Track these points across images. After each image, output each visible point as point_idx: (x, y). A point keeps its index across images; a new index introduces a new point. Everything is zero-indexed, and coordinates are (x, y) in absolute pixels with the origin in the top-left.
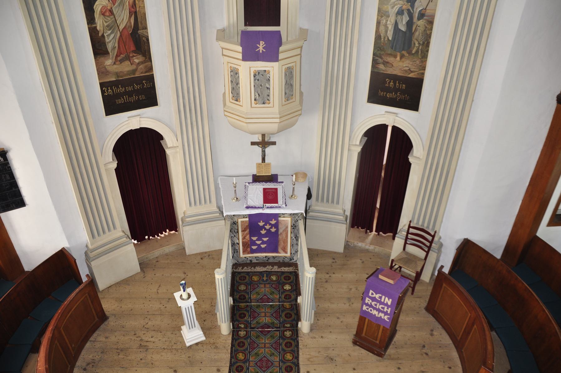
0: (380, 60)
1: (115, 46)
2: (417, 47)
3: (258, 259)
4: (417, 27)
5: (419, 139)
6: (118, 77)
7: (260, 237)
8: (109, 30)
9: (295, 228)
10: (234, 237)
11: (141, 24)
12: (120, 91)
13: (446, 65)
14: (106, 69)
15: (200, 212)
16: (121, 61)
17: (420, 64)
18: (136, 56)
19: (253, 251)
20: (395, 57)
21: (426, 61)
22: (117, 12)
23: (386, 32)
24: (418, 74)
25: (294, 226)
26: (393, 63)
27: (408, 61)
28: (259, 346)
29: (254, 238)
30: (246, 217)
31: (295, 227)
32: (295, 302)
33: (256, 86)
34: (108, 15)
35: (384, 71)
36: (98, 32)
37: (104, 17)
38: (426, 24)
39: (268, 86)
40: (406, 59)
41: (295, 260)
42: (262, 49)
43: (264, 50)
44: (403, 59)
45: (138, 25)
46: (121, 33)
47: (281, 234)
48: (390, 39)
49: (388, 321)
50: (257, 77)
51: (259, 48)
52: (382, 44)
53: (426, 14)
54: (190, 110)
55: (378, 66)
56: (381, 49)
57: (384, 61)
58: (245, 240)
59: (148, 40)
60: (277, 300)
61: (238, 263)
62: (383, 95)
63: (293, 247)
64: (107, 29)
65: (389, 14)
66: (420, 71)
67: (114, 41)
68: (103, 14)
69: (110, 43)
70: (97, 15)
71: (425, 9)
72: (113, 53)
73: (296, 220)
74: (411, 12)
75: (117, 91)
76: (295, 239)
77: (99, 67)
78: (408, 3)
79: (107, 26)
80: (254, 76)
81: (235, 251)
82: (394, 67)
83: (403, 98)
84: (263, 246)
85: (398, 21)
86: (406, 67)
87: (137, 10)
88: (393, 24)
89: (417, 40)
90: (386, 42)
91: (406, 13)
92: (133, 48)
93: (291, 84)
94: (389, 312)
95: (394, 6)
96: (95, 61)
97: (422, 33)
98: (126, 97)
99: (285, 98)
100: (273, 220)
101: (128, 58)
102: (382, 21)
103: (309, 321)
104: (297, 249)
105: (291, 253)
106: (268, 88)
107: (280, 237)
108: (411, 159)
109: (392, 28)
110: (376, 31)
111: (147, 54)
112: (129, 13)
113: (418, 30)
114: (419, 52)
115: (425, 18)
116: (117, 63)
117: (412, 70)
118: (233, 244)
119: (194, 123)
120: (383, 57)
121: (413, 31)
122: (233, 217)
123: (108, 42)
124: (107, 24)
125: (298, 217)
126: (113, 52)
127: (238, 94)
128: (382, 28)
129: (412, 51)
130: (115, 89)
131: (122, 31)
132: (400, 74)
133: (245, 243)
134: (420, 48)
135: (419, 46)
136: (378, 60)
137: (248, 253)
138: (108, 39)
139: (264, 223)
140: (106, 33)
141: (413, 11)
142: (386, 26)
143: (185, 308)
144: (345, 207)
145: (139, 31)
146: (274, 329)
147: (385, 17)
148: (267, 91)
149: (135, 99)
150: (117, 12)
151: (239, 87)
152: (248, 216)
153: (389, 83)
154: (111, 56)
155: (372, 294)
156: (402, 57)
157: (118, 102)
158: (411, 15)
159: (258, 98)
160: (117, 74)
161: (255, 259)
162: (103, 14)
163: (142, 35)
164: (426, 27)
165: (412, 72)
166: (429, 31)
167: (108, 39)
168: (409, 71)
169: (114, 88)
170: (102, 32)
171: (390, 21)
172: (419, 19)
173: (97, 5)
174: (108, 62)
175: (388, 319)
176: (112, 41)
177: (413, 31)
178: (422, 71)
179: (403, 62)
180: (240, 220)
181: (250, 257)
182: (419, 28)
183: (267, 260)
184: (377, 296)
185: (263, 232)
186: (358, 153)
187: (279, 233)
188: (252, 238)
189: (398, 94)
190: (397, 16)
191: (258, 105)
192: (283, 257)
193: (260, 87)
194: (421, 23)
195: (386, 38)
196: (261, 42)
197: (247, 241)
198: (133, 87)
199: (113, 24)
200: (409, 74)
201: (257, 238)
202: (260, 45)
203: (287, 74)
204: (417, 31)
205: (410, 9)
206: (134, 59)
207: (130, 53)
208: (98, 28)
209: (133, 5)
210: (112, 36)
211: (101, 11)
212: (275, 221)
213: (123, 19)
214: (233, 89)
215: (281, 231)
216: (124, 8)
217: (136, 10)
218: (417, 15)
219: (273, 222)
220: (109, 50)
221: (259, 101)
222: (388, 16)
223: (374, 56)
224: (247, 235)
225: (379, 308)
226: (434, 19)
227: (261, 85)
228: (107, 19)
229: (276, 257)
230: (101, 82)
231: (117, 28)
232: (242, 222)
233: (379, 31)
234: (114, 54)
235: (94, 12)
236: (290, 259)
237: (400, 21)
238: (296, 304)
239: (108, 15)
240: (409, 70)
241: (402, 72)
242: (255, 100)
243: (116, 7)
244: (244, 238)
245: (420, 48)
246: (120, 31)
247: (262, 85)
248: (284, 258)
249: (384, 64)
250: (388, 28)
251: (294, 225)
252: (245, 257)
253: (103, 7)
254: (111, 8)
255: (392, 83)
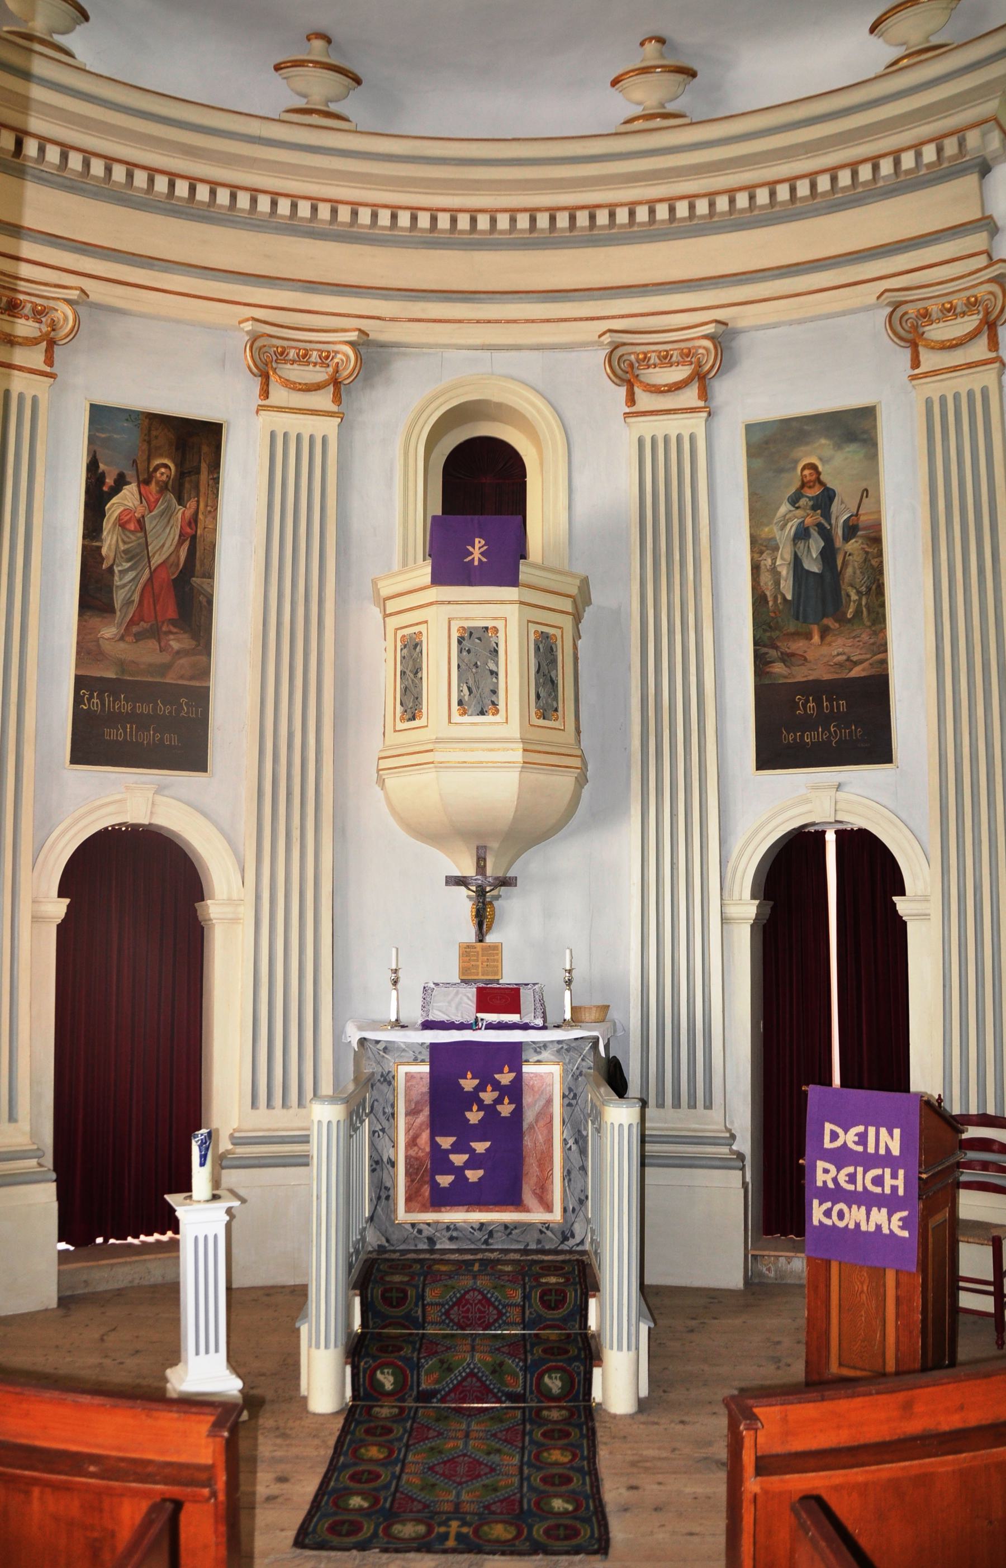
0: (773, 653)
1: (132, 599)
2: (854, 602)
3: (455, 1234)
4: (847, 558)
5: (911, 836)
6: (123, 672)
7: (465, 1135)
8: (128, 560)
9: (574, 1102)
10: (381, 1133)
11: (202, 564)
12: (120, 708)
13: (933, 620)
14: (99, 646)
15: (277, 1130)
16: (139, 637)
17: (872, 641)
18: (176, 633)
19: (441, 1199)
20: (808, 636)
21: (885, 628)
22: (154, 528)
23: (777, 583)
24: (871, 664)
25: (572, 1095)
26: (805, 652)
27: (840, 641)
28: (443, 1310)
29: (446, 1142)
30: (423, 1061)
31: (575, 1096)
32: (580, 1329)
33: (463, 667)
34: (133, 529)
35: (786, 677)
36: (102, 559)
37: (123, 532)
38: (865, 546)
39: (492, 666)
40: (835, 635)
41: (578, 1239)
42: (480, 556)
43: (484, 560)
44: (829, 639)
45: (194, 566)
46: (152, 573)
47: (531, 1127)
48: (789, 597)
49: (905, 1234)
50: (466, 644)
51: (472, 554)
52: (772, 614)
53: (861, 525)
54: (289, 794)
55: (768, 670)
56: (770, 627)
57: (782, 653)
58: (416, 1148)
59: (210, 602)
60: (514, 1314)
61: (387, 1245)
62: (795, 739)
63: (570, 1180)
64: (122, 558)
65: (777, 544)
66: (875, 657)
67: (133, 588)
68: (122, 523)
69: (122, 590)
70: (108, 524)
71: (857, 515)
72: (122, 615)
73: (578, 1072)
74: (826, 528)
75: (114, 707)
76: (574, 1147)
77: (83, 638)
78: (815, 511)
79: (125, 552)
80: (460, 642)
81: (383, 1194)
82: (810, 662)
83: (845, 736)
84: (473, 1175)
85: (799, 554)
86: (838, 655)
87: (199, 532)
88: (789, 564)
89: (852, 586)
90: (781, 607)
91: (814, 532)
92: (172, 612)
93: (551, 677)
94: (896, 1151)
95: (786, 524)
96: (79, 621)
97: (860, 568)
98: (131, 728)
99: (538, 708)
100: (506, 1069)
101: (155, 633)
102: (762, 563)
103: (629, 1349)
104: (584, 1190)
105: (565, 1210)
106: (494, 674)
107: (528, 1142)
108: (902, 905)
109: (788, 573)
110: (754, 588)
111: (202, 634)
112: (180, 536)
113: (851, 563)
114: (862, 612)
115: (860, 533)
116: (127, 639)
117: (855, 659)
118: (377, 1163)
119: (296, 834)
120: (779, 644)
121: (839, 569)
122: (381, 1053)
123: (117, 587)
124: (126, 546)
125: (583, 1060)
126: (124, 610)
127: (417, 699)
128: (766, 578)
129: (845, 613)
130: (109, 701)
131: (155, 570)
132: (826, 677)
133: (416, 1164)
134: (864, 602)
135: (860, 599)
136: (767, 653)
137: (424, 1209)
138: (121, 579)
139: (476, 1082)
140: (118, 566)
141: (830, 524)
142: (774, 571)
143: (196, 1238)
144: (732, 1123)
145: (194, 579)
146: (504, 1402)
147: (768, 551)
148: (488, 682)
149: (154, 739)
150: (154, 528)
151: (421, 678)
152: (426, 1055)
153: (804, 706)
154: (117, 619)
155: (834, 1136)
156: (824, 632)
157: (110, 736)
158: (826, 535)
159: (466, 698)
160: (122, 665)
161: (444, 1232)
162: (122, 523)
163: (200, 588)
164: (867, 553)
165: (856, 663)
166: (876, 560)
167: (121, 579)
168: (847, 663)
169: (109, 696)
170: (110, 562)
171: (782, 558)
172: (846, 539)
173: (114, 504)
174: (109, 632)
175: (902, 1228)
176: (128, 587)
177: (839, 569)
178: (880, 656)
179: (830, 644)
180: (403, 1070)
181: (429, 1224)
182: (851, 557)
183: (486, 1242)
184: (849, 1138)
185: (474, 1116)
186: (752, 926)
187: (525, 1126)
188: (439, 1139)
189: (832, 730)
190: (795, 545)
191: (466, 719)
192: (540, 1226)
193: (474, 670)
194: (854, 546)
195: (779, 597)
196: (477, 540)
197: (421, 1154)
198: (155, 709)
199: (138, 550)
200: (851, 670)
201: (454, 1139)
202: (474, 548)
203: (541, 646)
204: (847, 565)
205: (823, 521)
206: (169, 640)
207: (163, 622)
208: (104, 551)
209: (192, 521)
210: (131, 575)
211: (119, 518)
212: (513, 1075)
213: (163, 545)
214: (405, 690)
215: (529, 1116)
216: (172, 522)
217: (196, 532)
218: (840, 532)
219: (505, 1078)
220: (118, 604)
221: (470, 707)
222: (776, 548)
223: (758, 648)
224: (423, 1131)
225: (864, 1187)
226: (880, 530)
227: (476, 664)
228: (129, 537)
229: (515, 1228)
230: (80, 673)
231: (147, 560)
232: (409, 1076)
233: (759, 585)
234: (124, 616)
235: (105, 516)
236: (563, 1232)
237: (805, 553)
238: (586, 1334)
239: (133, 529)
240: (848, 659)
241: (833, 670)
242: (459, 705)
243: (154, 517)
244: (412, 1142)
245: (864, 602)
246: (150, 569)
247: (479, 663)
248: (541, 1232)
249: (784, 661)
250: (779, 573)
251: (570, 1090)
252: (413, 1225)
253: (125, 510)
254: (143, 517)
255: (811, 704)
